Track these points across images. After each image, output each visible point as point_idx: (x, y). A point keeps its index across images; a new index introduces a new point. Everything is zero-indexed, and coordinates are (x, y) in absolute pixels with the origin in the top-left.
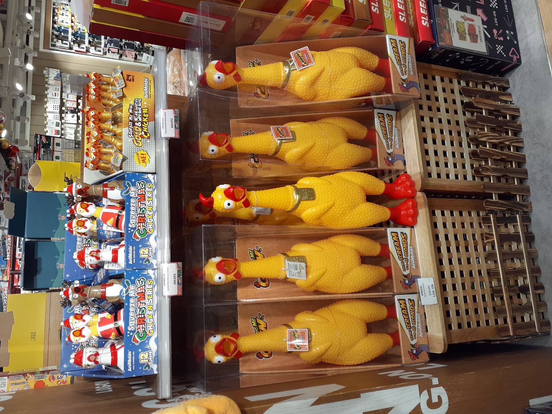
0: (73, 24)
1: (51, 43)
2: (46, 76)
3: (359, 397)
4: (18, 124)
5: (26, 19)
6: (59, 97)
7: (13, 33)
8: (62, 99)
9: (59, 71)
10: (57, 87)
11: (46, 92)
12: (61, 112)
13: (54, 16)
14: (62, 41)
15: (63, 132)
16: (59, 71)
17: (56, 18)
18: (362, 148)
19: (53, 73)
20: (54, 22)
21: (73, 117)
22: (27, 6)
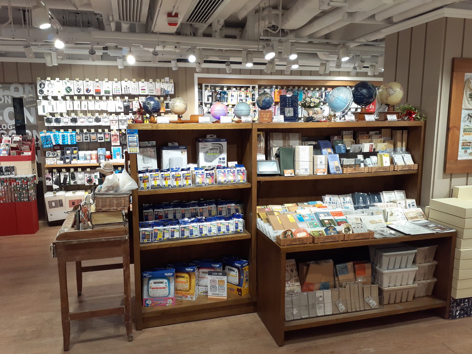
0: (230, 106)
1: (209, 85)
2: (162, 80)
3: (368, 208)
4: (87, 52)
5: (268, 52)
6: (141, 93)
7: (178, 43)
8: (138, 96)
9: (173, 93)
10: (154, 91)
11: (151, 80)
12: (122, 96)
13: (236, 87)
14: (211, 96)
15: (97, 98)
16: (173, 93)
17: (234, 89)
18: (123, 282)
19: (169, 88)
20: (229, 88)
21: (119, 108)
22: (231, 60)
